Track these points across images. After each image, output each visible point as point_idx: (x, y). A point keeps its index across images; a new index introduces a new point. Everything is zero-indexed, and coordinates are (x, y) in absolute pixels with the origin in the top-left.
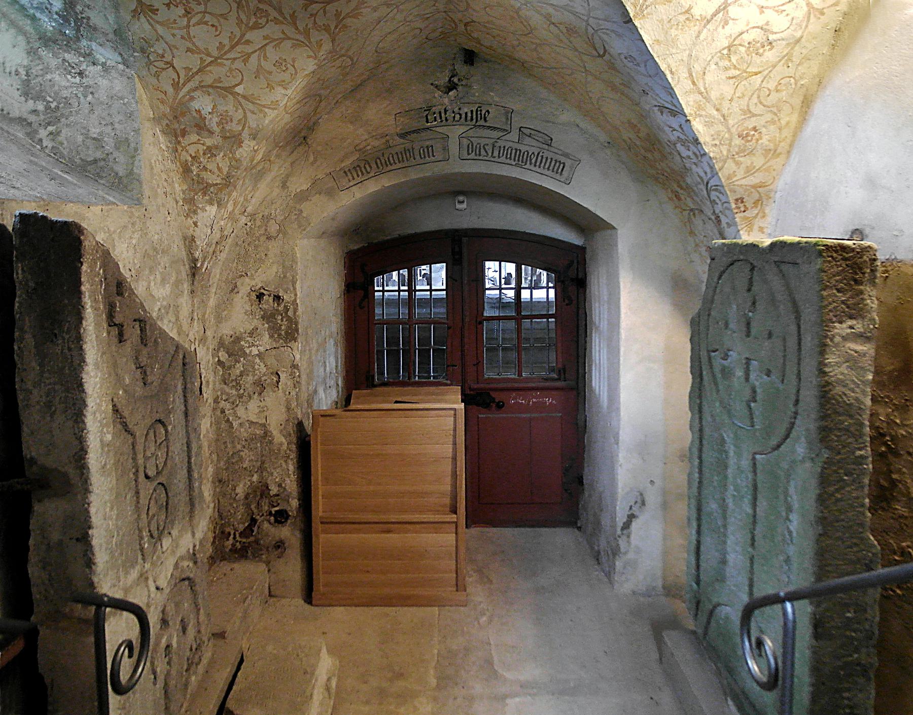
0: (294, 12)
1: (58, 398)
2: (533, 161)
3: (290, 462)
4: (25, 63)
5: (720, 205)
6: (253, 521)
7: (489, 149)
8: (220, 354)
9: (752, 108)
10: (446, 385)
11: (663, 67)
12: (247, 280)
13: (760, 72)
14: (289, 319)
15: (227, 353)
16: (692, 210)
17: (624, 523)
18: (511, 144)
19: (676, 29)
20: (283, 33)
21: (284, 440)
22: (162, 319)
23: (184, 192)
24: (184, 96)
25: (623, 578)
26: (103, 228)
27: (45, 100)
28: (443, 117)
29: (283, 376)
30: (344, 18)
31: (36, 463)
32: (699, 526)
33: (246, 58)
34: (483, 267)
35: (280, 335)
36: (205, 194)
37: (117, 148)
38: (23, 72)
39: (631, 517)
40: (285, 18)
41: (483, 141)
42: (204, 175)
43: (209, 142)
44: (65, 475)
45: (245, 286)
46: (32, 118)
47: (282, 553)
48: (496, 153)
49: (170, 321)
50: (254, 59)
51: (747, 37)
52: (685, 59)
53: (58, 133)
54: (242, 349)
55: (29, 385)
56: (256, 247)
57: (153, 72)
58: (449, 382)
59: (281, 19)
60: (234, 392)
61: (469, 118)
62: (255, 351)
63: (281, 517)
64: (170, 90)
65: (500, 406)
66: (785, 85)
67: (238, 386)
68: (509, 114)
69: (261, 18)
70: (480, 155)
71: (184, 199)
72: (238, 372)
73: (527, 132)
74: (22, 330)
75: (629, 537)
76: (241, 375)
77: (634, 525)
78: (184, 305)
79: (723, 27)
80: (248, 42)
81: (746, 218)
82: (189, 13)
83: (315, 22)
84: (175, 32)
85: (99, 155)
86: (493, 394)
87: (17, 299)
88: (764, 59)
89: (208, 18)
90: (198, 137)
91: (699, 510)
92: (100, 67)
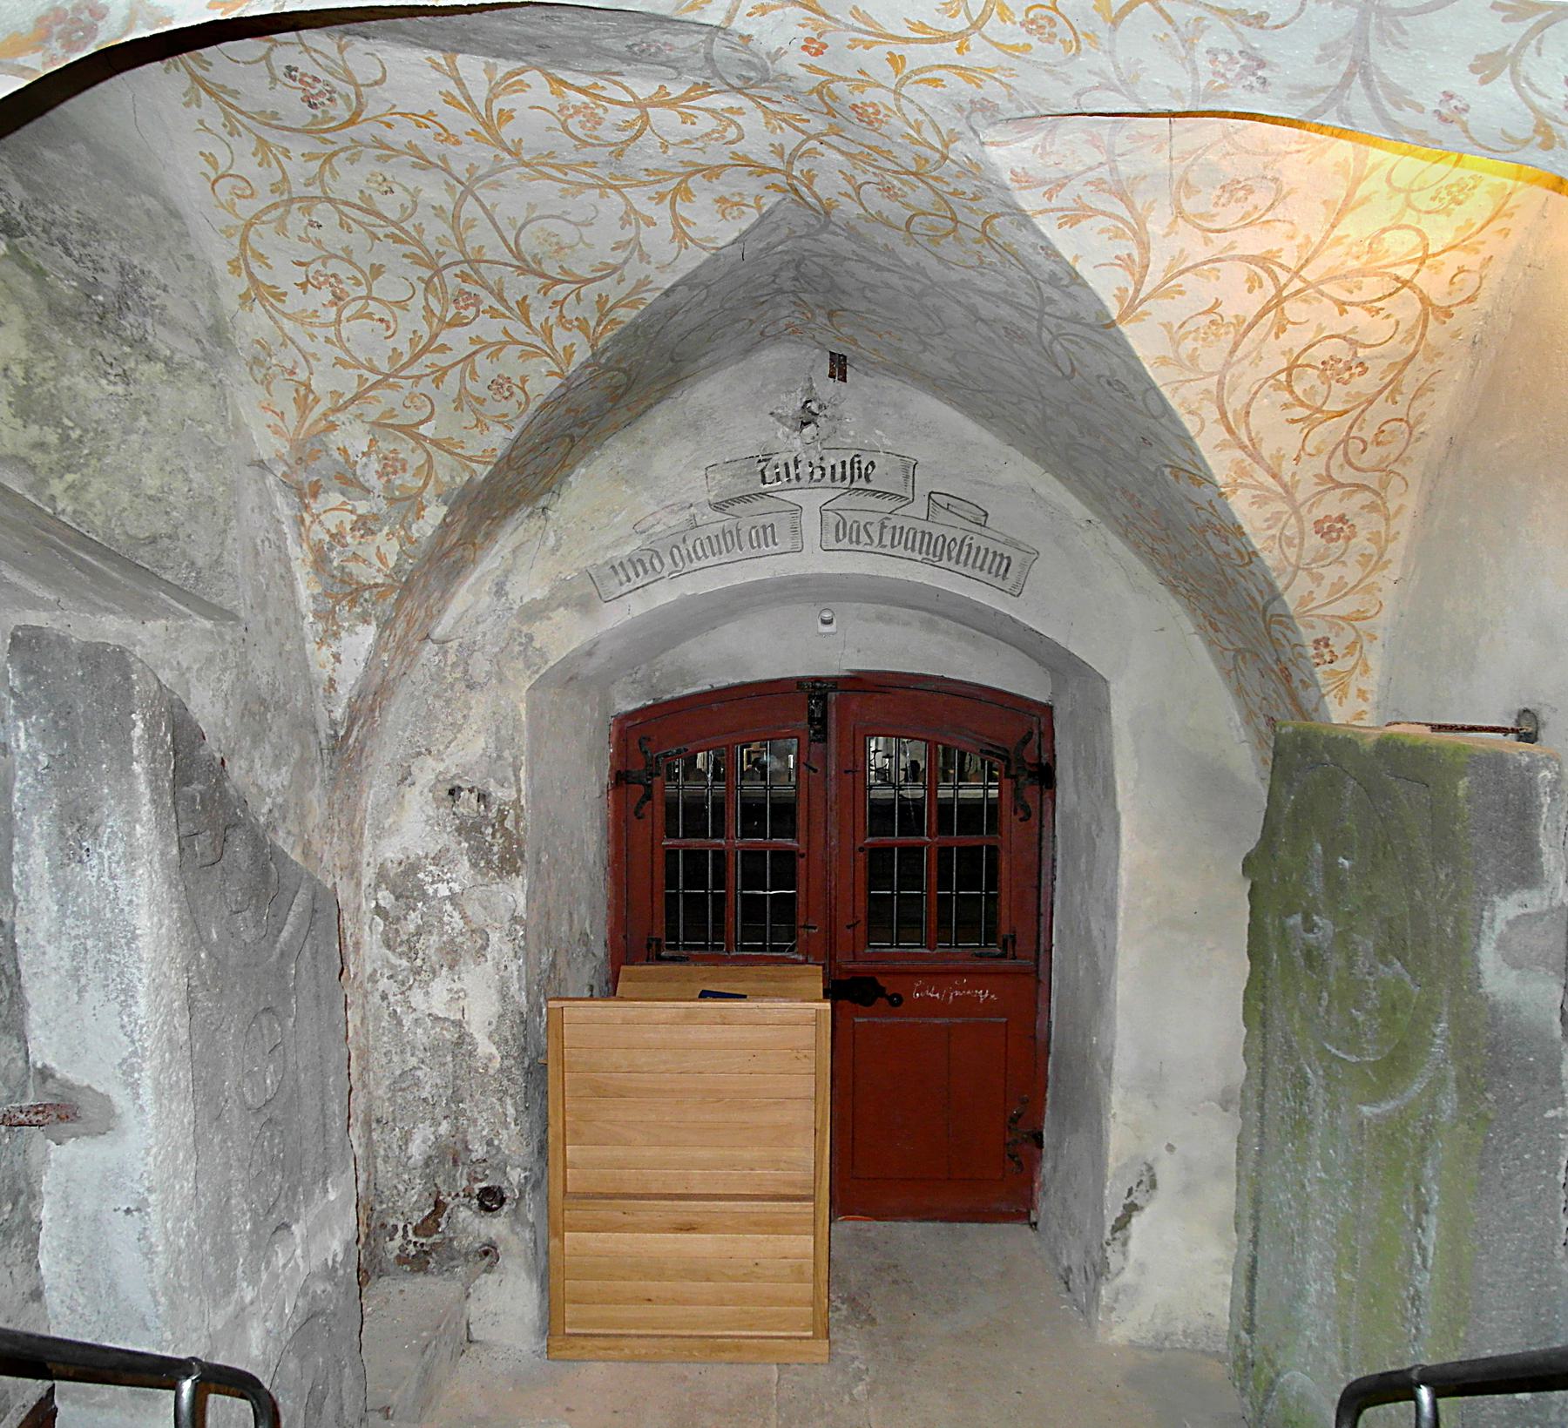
0: (525, 298)
1: (91, 962)
2: (954, 554)
3: (509, 1101)
4: (23, 355)
5: (1288, 648)
6: (439, 1206)
7: (874, 531)
8: (380, 895)
9: (1335, 474)
10: (795, 962)
11: (1174, 403)
12: (430, 761)
13: (1346, 412)
14: (506, 833)
15: (393, 892)
16: (1238, 651)
17: (1117, 1220)
18: (915, 523)
19: (1195, 339)
20: (506, 332)
21: (494, 1050)
22: (275, 829)
23: (315, 598)
24: (317, 422)
25: (1113, 1316)
26: (169, 662)
27: (59, 424)
28: (789, 472)
29: (494, 937)
30: (611, 309)
31: (53, 1076)
32: (1256, 1230)
33: (440, 375)
34: (866, 747)
35: (489, 862)
36: (353, 603)
37: (193, 517)
38: (17, 371)
39: (1131, 1209)
40: (510, 309)
41: (863, 518)
42: (352, 567)
43: (363, 507)
44: (106, 1098)
45: (427, 772)
46: (37, 458)
47: (491, 1265)
48: (887, 540)
49: (289, 833)
50: (452, 378)
51: (1320, 353)
52: (1214, 389)
53: (85, 487)
54: (420, 886)
55: (40, 937)
56: (448, 702)
57: (260, 377)
58: (801, 958)
59: (502, 309)
60: (404, 963)
61: (838, 476)
62: (443, 890)
63: (490, 1200)
64: (292, 413)
65: (896, 1001)
66: (1392, 432)
67: (412, 952)
68: (910, 469)
69: (466, 307)
70: (858, 542)
71: (316, 614)
72: (412, 928)
73: (943, 500)
74: (26, 841)
75: (1125, 1244)
76: (418, 934)
77: (1137, 1222)
78: (315, 804)
79: (1277, 337)
80: (443, 348)
81: (1334, 673)
82: (340, 299)
83: (562, 316)
84: (316, 331)
85: (162, 526)
86: (882, 981)
87: (17, 785)
88: (1352, 388)
89: (373, 306)
90: (342, 499)
91: (1256, 1202)
92: (160, 366)
